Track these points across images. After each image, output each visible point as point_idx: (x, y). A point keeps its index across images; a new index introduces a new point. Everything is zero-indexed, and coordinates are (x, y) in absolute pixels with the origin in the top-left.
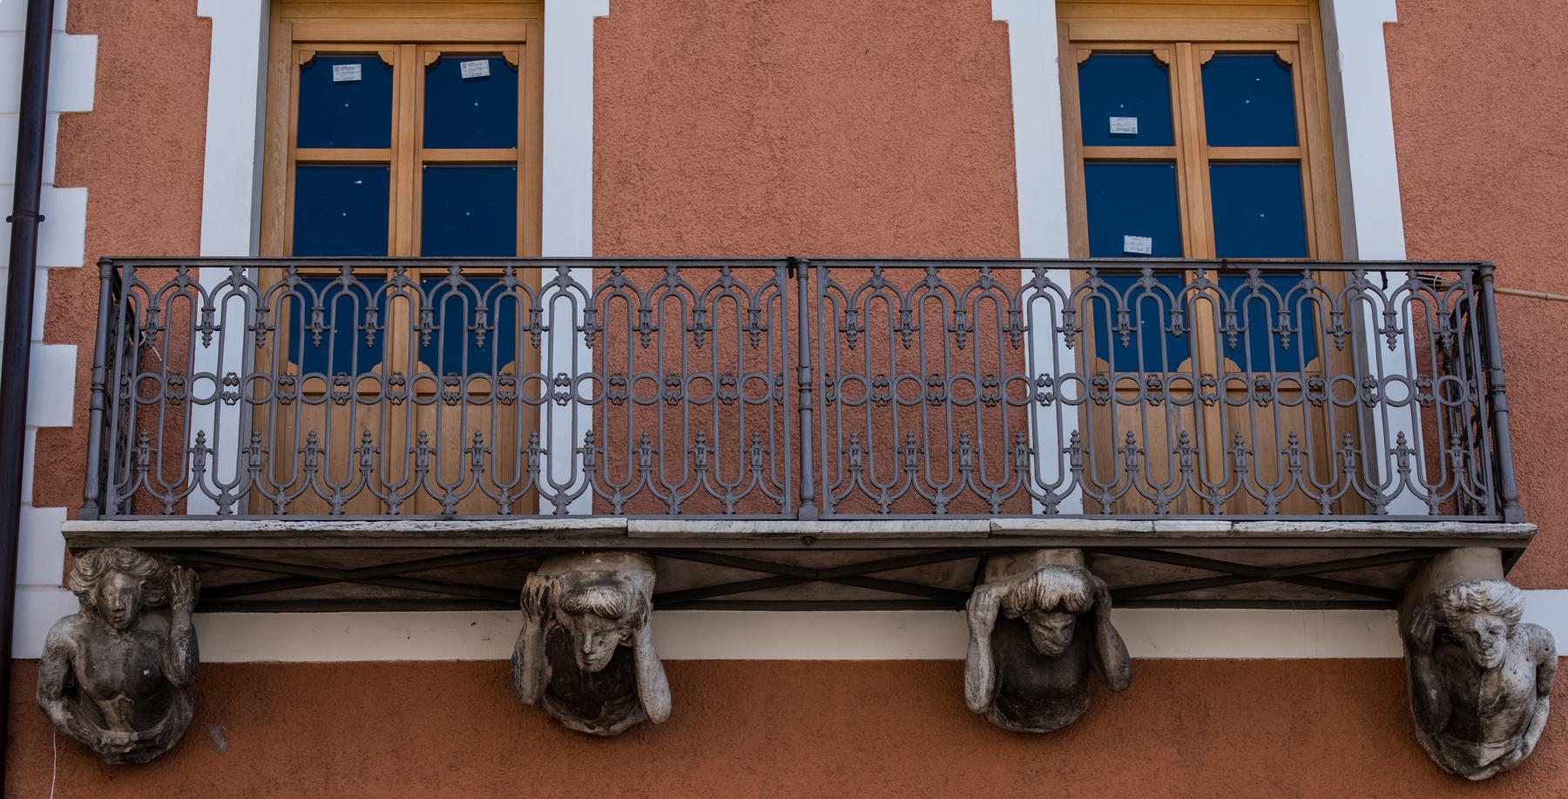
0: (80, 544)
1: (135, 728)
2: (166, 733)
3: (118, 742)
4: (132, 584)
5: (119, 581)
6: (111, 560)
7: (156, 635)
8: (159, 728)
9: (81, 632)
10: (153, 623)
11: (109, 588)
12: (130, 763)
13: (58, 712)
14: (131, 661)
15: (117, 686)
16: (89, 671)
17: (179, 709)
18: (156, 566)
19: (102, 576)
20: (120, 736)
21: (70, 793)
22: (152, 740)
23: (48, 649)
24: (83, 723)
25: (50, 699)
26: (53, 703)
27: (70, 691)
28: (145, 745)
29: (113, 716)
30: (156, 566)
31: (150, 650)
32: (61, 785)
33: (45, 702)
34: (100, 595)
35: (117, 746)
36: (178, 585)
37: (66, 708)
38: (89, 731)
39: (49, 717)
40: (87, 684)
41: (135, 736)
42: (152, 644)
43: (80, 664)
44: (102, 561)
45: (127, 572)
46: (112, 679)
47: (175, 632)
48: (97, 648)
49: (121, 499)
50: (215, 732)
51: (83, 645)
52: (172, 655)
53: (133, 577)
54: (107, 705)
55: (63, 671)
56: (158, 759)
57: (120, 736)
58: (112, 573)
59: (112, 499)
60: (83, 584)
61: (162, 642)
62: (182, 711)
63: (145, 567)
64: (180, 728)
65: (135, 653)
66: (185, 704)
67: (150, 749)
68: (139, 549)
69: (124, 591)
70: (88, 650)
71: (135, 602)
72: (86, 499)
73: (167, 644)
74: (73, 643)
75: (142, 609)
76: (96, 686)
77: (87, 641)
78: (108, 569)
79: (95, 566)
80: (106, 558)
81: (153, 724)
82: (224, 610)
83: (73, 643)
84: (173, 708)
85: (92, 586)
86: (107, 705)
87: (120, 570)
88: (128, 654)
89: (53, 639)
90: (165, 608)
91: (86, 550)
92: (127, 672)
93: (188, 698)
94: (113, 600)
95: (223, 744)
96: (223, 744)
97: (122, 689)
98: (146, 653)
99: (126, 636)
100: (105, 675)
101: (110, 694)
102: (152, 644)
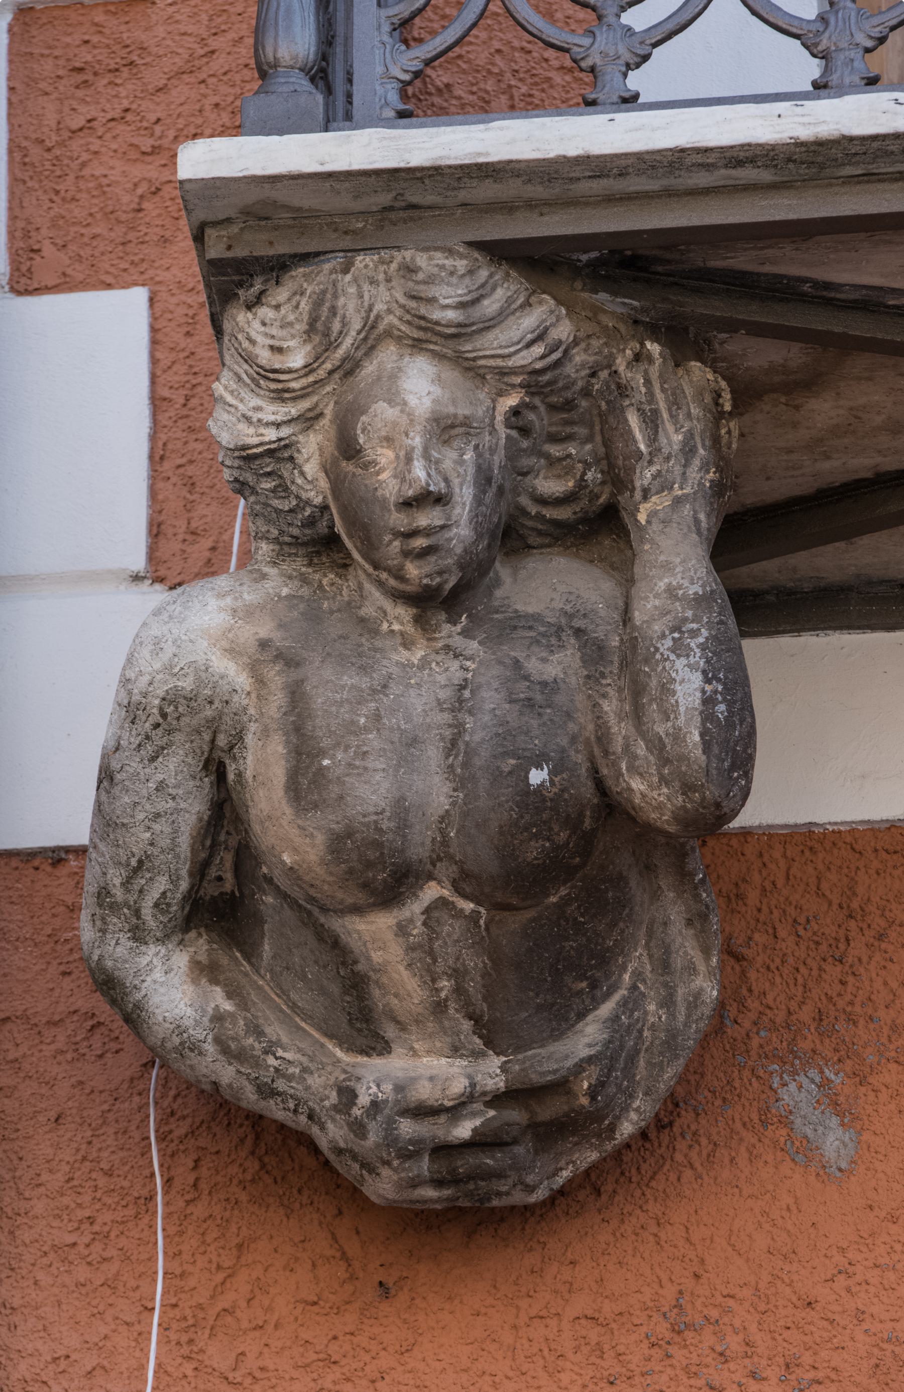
0: (257, 244)
1: (492, 1035)
2: (615, 1057)
3: (424, 1092)
4: (472, 403)
5: (420, 385)
6: (385, 299)
7: (572, 628)
8: (587, 1037)
9: (265, 629)
10: (552, 584)
11: (383, 412)
12: (471, 1206)
13: (172, 988)
14: (478, 730)
15: (420, 844)
16: (306, 782)
17: (664, 966)
18: (563, 331)
19: (349, 369)
20: (432, 1068)
21: (218, 1355)
22: (561, 1086)
23: (131, 711)
24: (274, 1030)
25: (138, 934)
26: (152, 954)
27: (223, 900)
28: (541, 1114)
29: (401, 983)
30: (563, 331)
31: (549, 687)
32: (185, 1331)
33: (117, 951)
34: (348, 448)
35: (422, 1112)
36: (652, 421)
37: (206, 971)
38: (307, 1066)
39: (133, 1018)
40: (289, 838)
41: (492, 1072)
42: (559, 665)
43: (263, 766)
44: (350, 306)
45: (446, 342)
46: (402, 810)
47: (648, 607)
48: (332, 687)
49: (410, 59)
50: (797, 1094)
51: (276, 677)
52: (640, 689)
53: (472, 369)
54: (378, 937)
55: (192, 808)
56: (590, 1181)
57: (432, 1068)
58: (388, 355)
59: (377, 61)
60: (273, 412)
61: (594, 653)
62: (671, 970)
63: (527, 326)
64: (671, 1044)
65: (491, 699)
66: (685, 945)
67: (552, 1134)
68: (500, 253)
69: (445, 429)
70: (297, 696)
71: (483, 478)
72: (265, 71)
73: (624, 662)
74: (234, 675)
75: (511, 535)
76: (338, 842)
77: (289, 661)
78: (372, 337)
79: (320, 330)
80: (365, 289)
81: (563, 1017)
82: (798, 626)
83: (234, 675)
84: (637, 961)
85: (309, 420)
86: (378, 937)
87: (426, 337)
88: (461, 700)
89: (150, 664)
90: (601, 526)
91: (278, 268)
92: (462, 780)
93: (698, 919)
94: (396, 466)
95: (834, 1141)
96: (834, 1141)
97: (442, 852)
98: (537, 698)
99: (449, 632)
100: (370, 791)
101: (384, 876)
102: (559, 665)
